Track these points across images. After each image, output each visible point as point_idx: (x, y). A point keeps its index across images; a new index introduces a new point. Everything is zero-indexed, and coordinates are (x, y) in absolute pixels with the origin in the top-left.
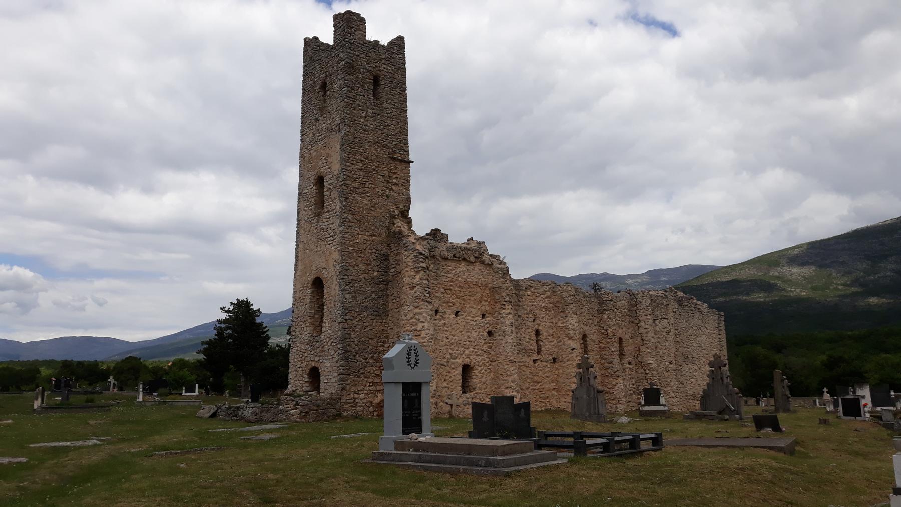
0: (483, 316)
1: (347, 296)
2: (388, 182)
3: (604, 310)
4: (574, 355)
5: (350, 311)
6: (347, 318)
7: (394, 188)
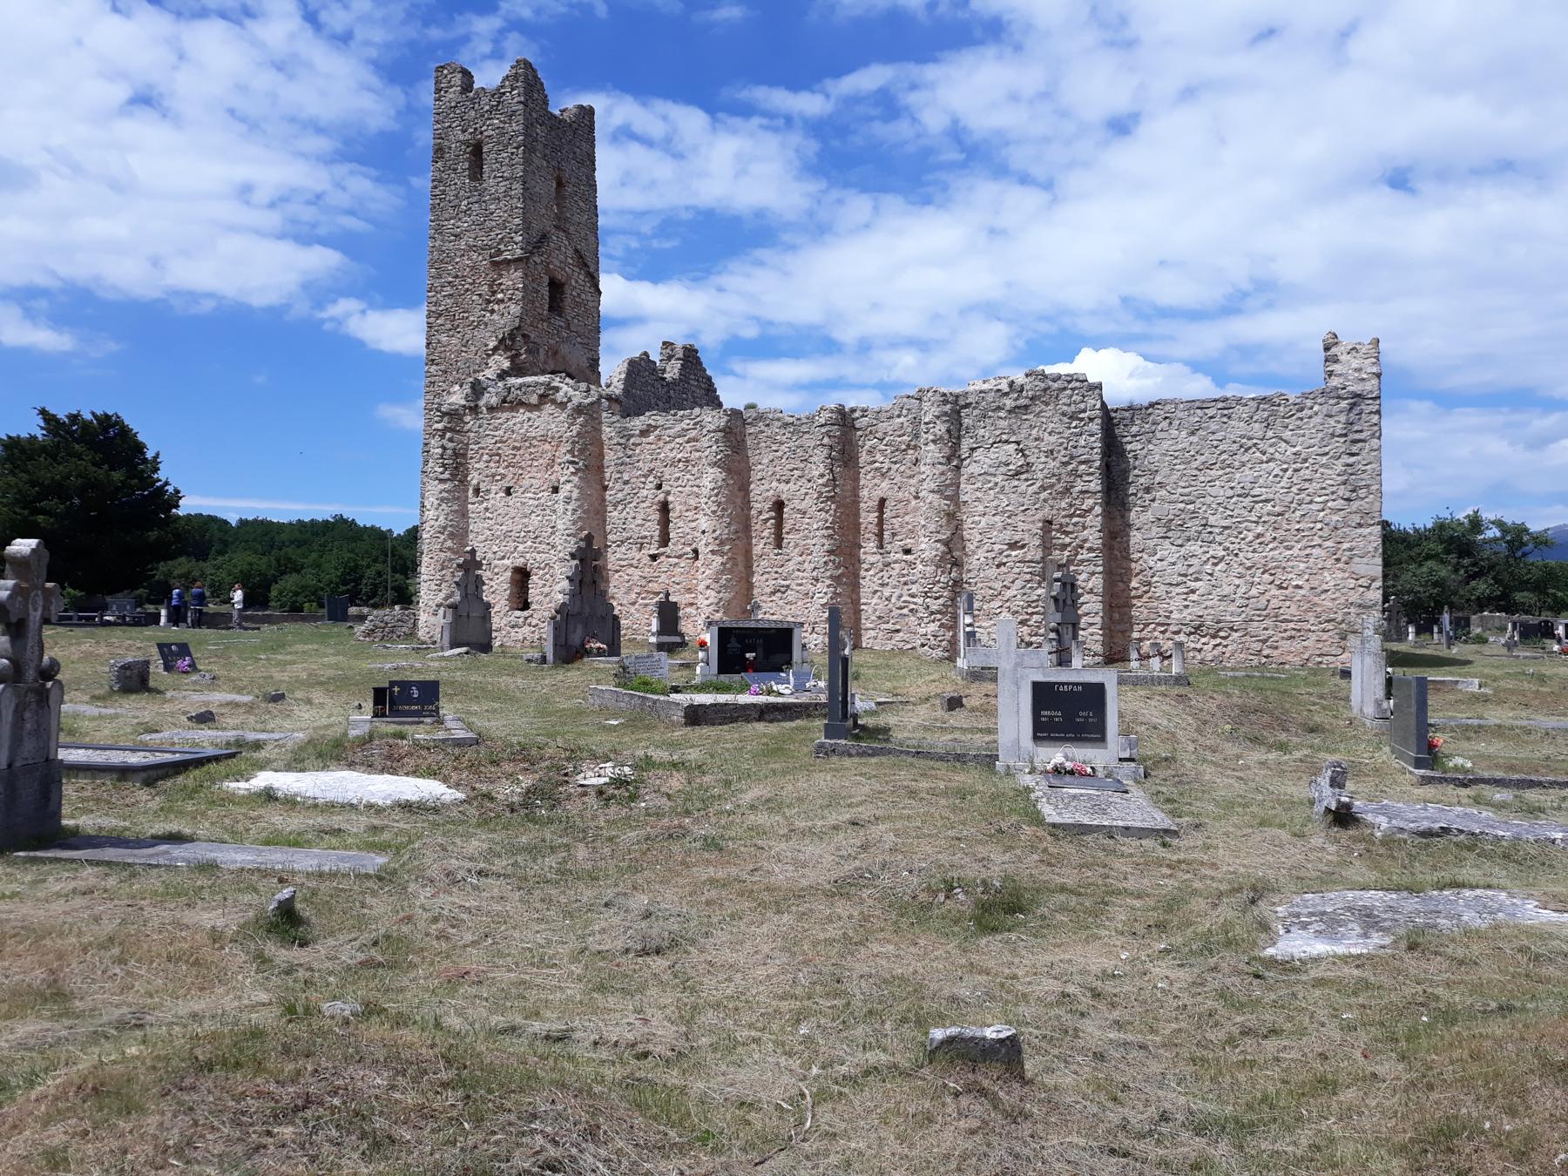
2: (489, 302)
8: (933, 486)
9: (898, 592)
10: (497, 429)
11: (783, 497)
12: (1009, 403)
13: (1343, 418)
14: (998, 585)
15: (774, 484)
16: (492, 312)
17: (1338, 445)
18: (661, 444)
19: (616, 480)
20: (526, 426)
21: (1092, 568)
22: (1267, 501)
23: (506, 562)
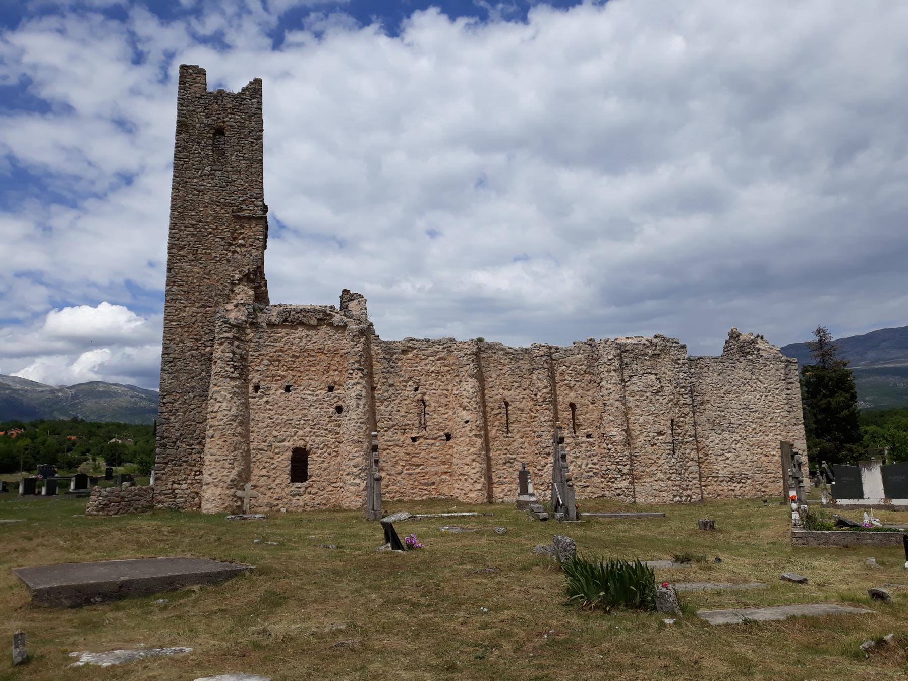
0: (331, 389)
1: (166, 376)
2: (231, 244)
3: (534, 369)
4: (468, 428)
5: (170, 393)
6: (165, 401)
7: (238, 249)
8: (618, 397)
9: (585, 462)
10: (276, 341)
11: (508, 399)
12: (651, 352)
13: (783, 372)
14: (654, 457)
15: (501, 391)
16: (234, 252)
17: (782, 385)
18: (418, 360)
19: (383, 384)
20: (304, 340)
21: (691, 447)
22: (756, 411)
23: (286, 444)
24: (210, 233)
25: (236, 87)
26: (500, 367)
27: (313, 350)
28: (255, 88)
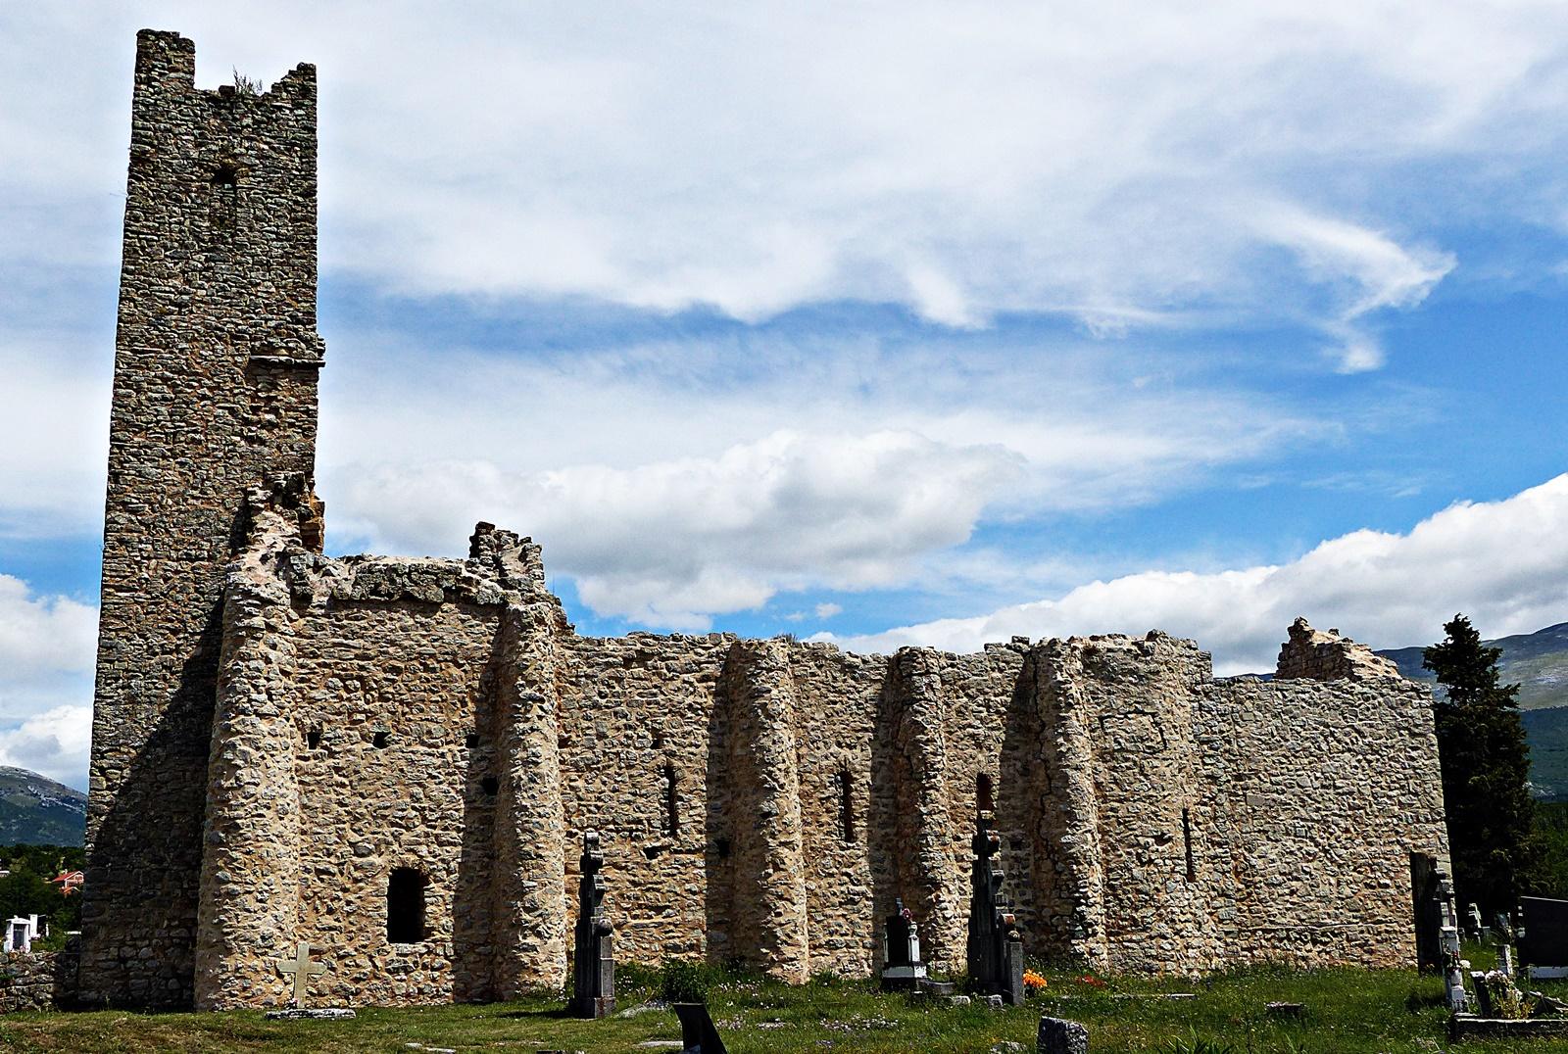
15: (834, 749)
24: (204, 397)
25: (265, 77)
26: (831, 697)
27: (432, 656)
28: (302, 82)
